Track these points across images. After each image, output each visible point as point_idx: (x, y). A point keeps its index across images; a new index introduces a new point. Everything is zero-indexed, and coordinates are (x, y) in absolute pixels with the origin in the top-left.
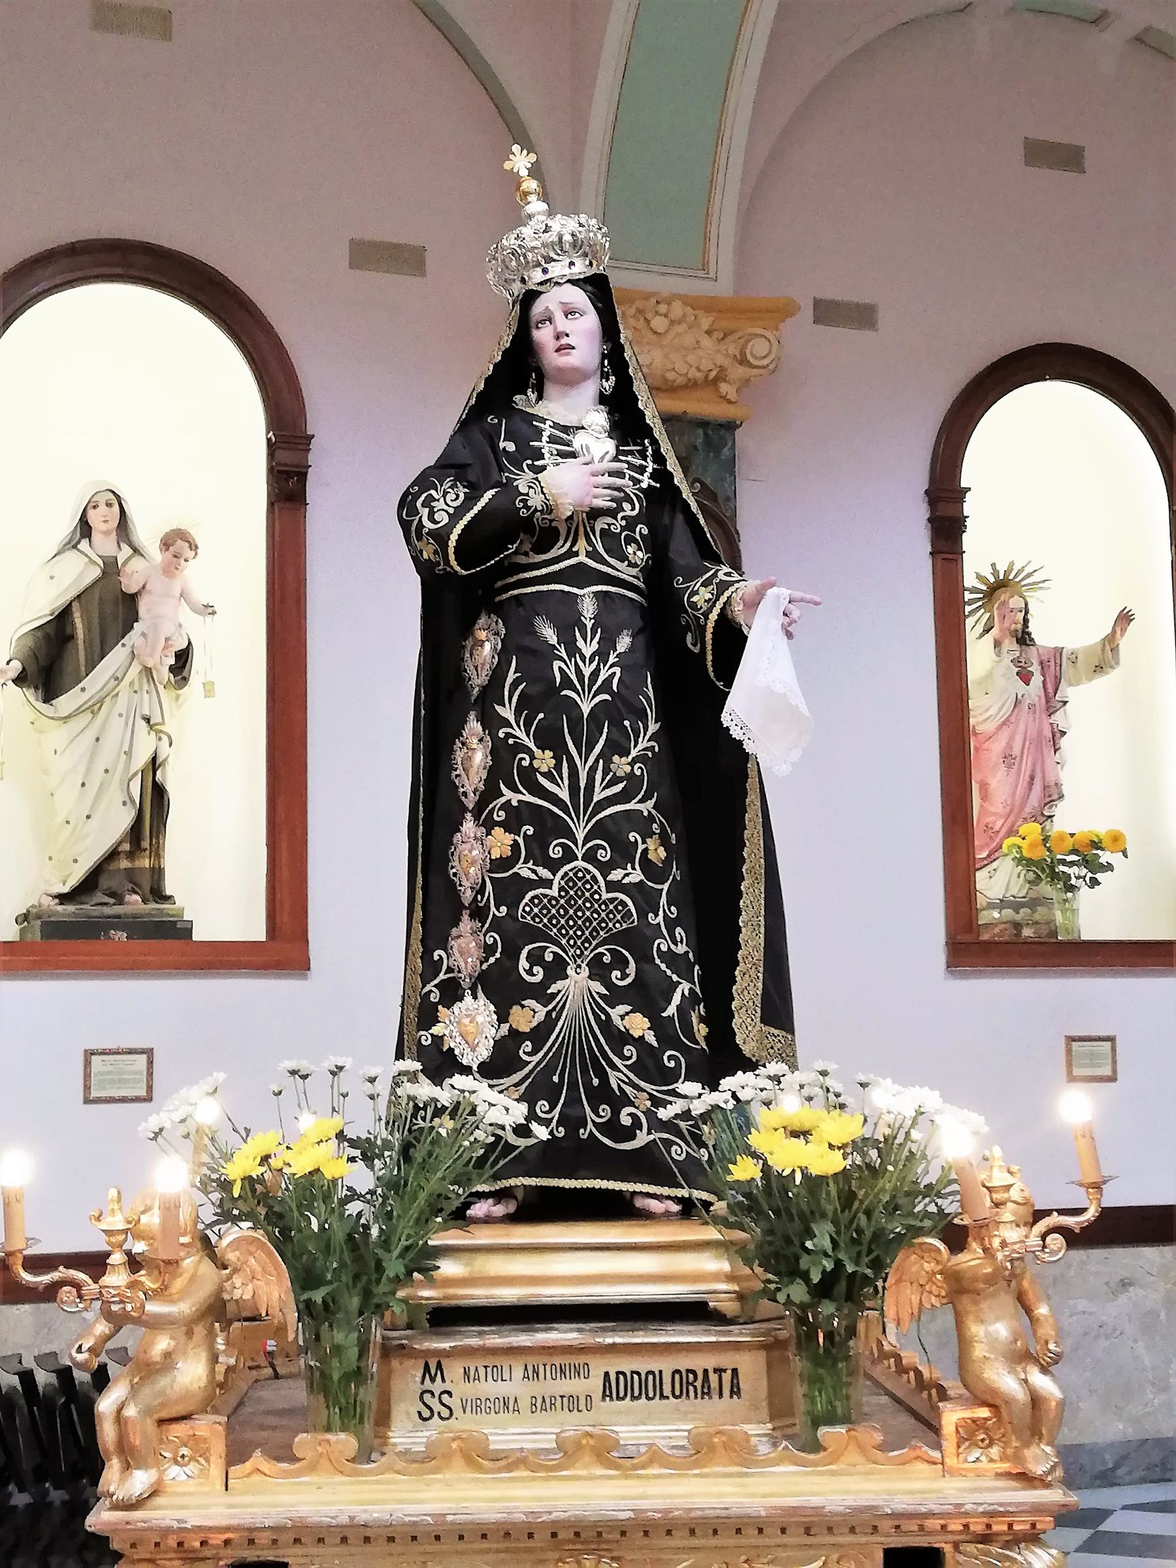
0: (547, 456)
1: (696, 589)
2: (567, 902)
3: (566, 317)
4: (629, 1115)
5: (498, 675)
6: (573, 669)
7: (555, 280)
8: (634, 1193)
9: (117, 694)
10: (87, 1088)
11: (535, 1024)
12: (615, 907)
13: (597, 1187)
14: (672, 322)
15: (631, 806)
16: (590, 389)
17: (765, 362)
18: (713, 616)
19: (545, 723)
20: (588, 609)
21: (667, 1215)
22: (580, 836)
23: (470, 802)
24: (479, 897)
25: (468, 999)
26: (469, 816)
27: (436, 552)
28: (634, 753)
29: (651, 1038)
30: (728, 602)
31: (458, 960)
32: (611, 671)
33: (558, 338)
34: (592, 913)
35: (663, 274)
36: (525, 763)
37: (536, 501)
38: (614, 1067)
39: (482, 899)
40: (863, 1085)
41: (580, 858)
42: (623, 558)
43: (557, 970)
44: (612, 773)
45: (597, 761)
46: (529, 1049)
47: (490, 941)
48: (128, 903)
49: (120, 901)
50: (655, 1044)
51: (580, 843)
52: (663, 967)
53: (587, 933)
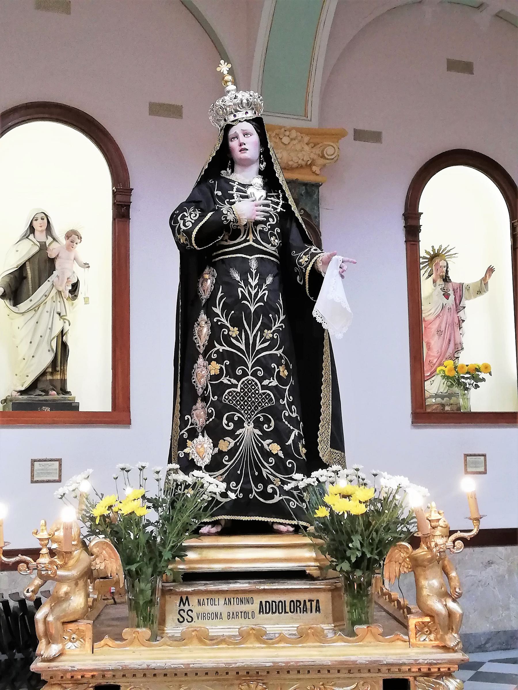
0: (235, 198)
7: (239, 120)
8: (273, 523)
9: (46, 302)
10: (32, 476)
11: (229, 448)
12: (266, 397)
14: (292, 139)
18: (309, 268)
19: (234, 315)
20: (254, 265)
21: (288, 532)
22: (250, 366)
23: (201, 350)
25: (200, 437)
26: (201, 356)
28: (274, 329)
29: (281, 454)
31: (195, 419)
32: (264, 293)
36: (226, 333)
40: (375, 475)
42: (269, 242)
43: (239, 424)
45: (257, 332)
47: (210, 411)
48: (51, 395)
49: (47, 393)
50: (283, 457)
51: (250, 368)
52: (286, 423)
53: (253, 408)
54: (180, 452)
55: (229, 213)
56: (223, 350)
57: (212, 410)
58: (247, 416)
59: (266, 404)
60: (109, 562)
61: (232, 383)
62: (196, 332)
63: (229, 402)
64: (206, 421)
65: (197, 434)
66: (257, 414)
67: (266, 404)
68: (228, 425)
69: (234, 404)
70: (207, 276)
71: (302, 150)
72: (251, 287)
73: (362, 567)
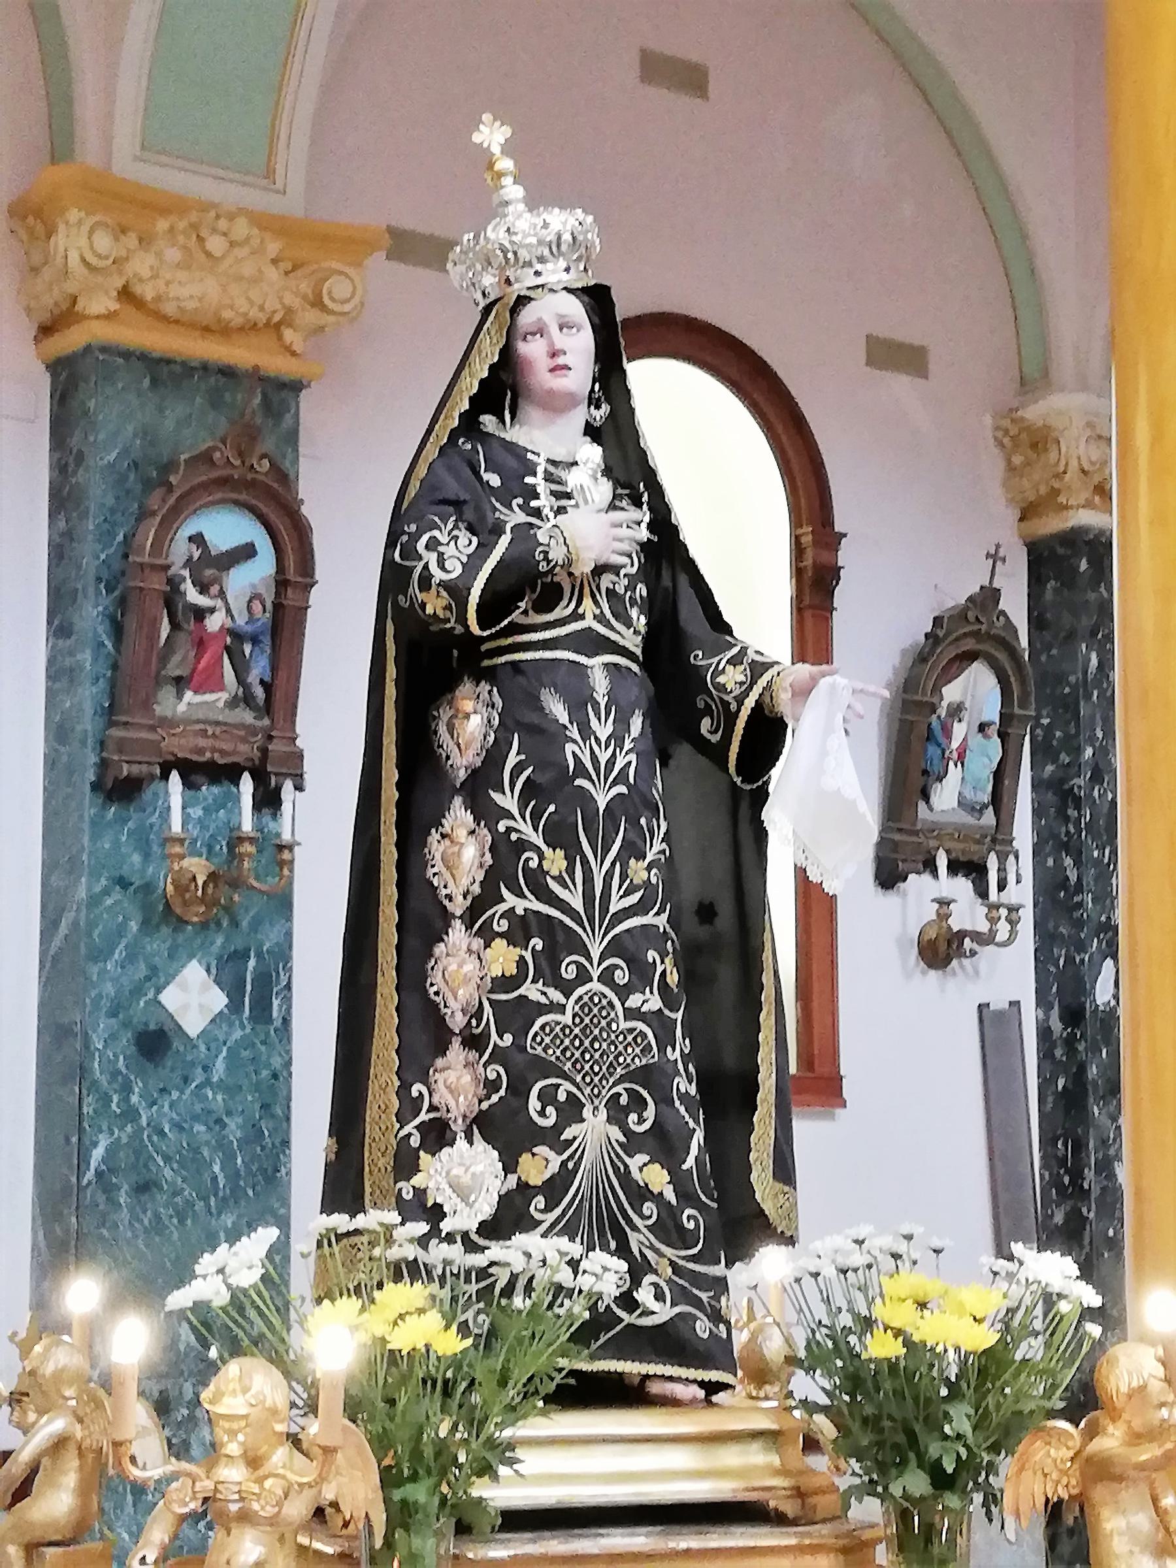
0: (542, 496)
1: (721, 667)
3: (561, 329)
4: (652, 1284)
5: (494, 757)
6: (587, 752)
7: (549, 286)
8: (646, 1377)
11: (547, 1175)
12: (635, 1039)
14: (232, 244)
15: (648, 919)
17: (347, 308)
18: (750, 702)
19: (556, 817)
20: (600, 684)
21: (693, 1402)
22: (595, 954)
23: (458, 906)
24: (474, 1022)
25: (461, 1143)
26: (458, 924)
28: (649, 857)
29: (670, 1195)
30: (769, 686)
31: (442, 1096)
32: (626, 759)
33: (554, 355)
34: (609, 1045)
36: (534, 864)
37: (557, 554)
38: (635, 1228)
39: (478, 1026)
41: (595, 978)
42: (628, 623)
43: (572, 1111)
45: (613, 864)
46: (542, 1206)
47: (492, 1076)
50: (674, 1201)
51: (595, 961)
52: (682, 1110)
53: (604, 1068)
54: (400, 1185)
56: (525, 910)
58: (592, 1090)
59: (637, 1060)
61: (552, 1002)
62: (438, 856)
63: (545, 1050)
64: (480, 1101)
65: (448, 1134)
66: (614, 1085)
67: (637, 1060)
68: (542, 1113)
69: (558, 1058)
70: (468, 705)
71: (257, 280)
73: (313, 1525)
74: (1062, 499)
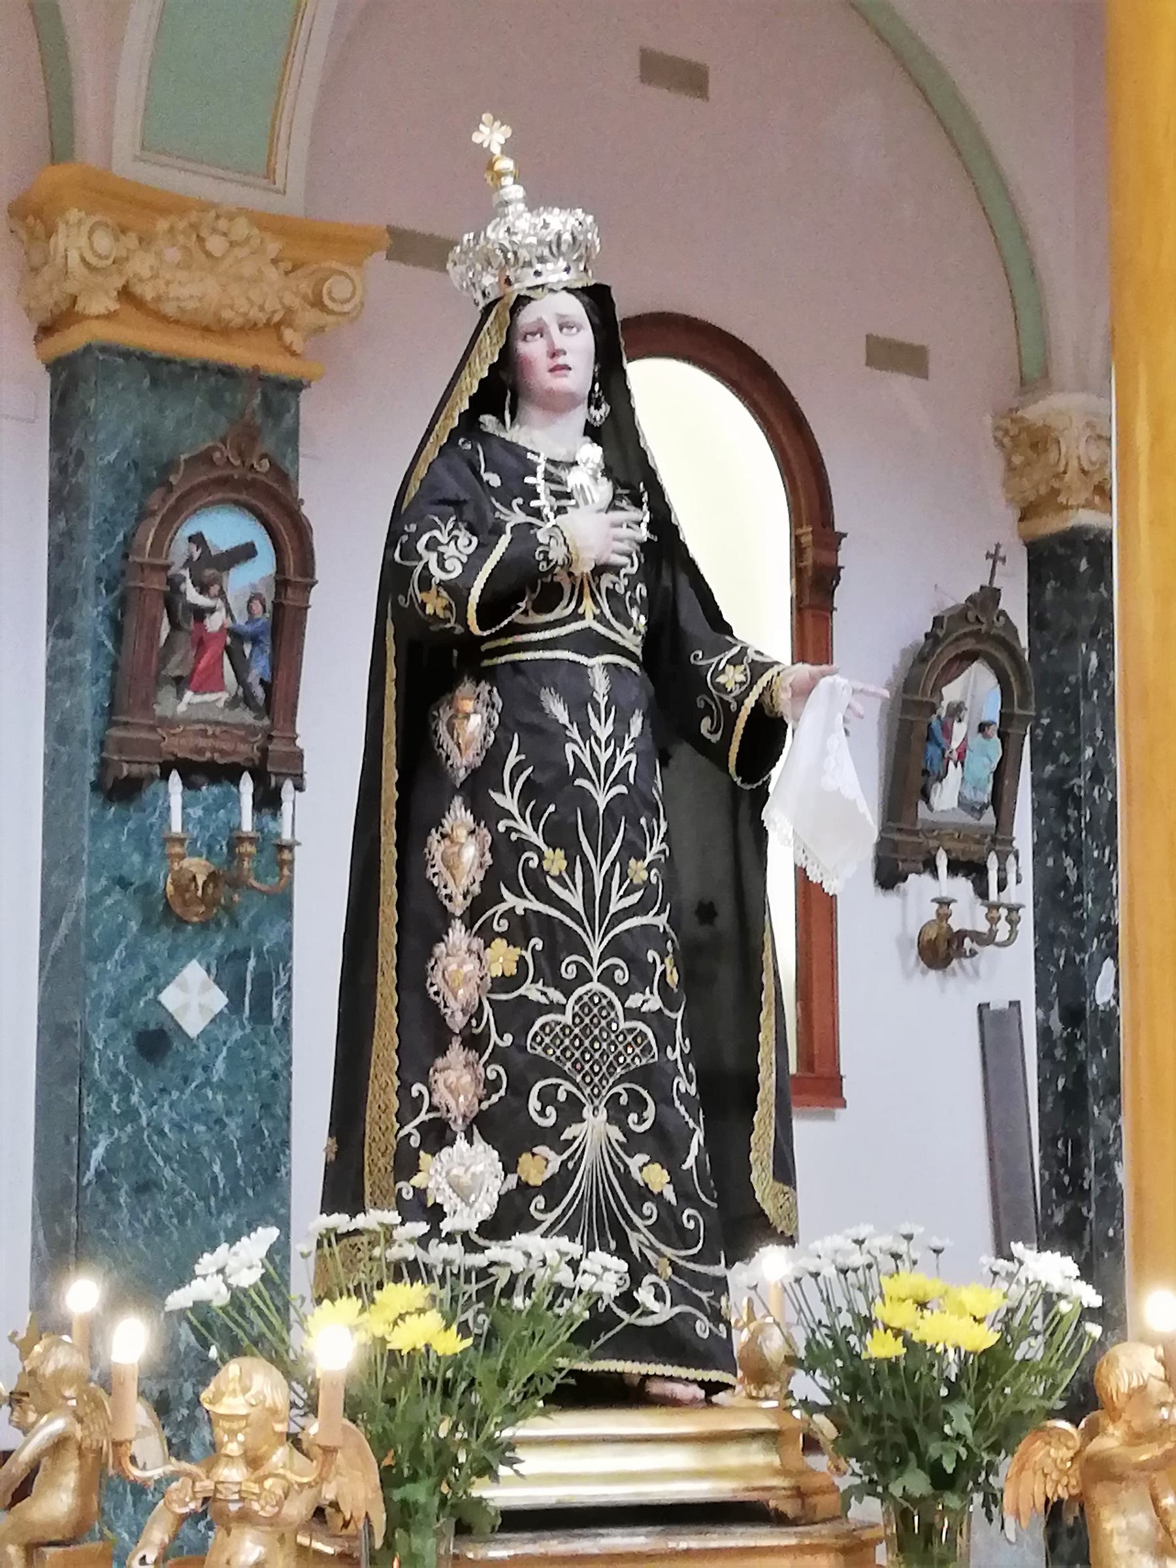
0: (542, 496)
1: (721, 667)
2: (583, 1031)
5: (494, 757)
8: (647, 1377)
11: (547, 1175)
12: (635, 1039)
13: (692, 1370)
14: (232, 244)
15: (648, 919)
16: (579, 416)
17: (347, 308)
18: (750, 702)
19: (556, 817)
20: (601, 684)
21: (692, 1403)
22: (595, 954)
23: (458, 906)
24: (474, 1022)
25: (461, 1143)
26: (458, 924)
27: (448, 608)
28: (649, 857)
29: (670, 1195)
31: (442, 1096)
35: (244, 184)
36: (534, 864)
37: (557, 554)
38: (635, 1228)
39: (478, 1026)
40: (937, 1251)
41: (595, 978)
42: (628, 623)
43: (572, 1111)
44: (628, 881)
45: (613, 864)
46: (542, 1206)
47: (492, 1076)
50: (674, 1201)
51: (595, 961)
52: (682, 1110)
54: (400, 1184)
55: (553, 542)
56: (525, 910)
57: (498, 1073)
60: (346, 1480)
61: (552, 1002)
62: (438, 856)
63: (545, 1050)
64: (480, 1101)
65: (448, 1134)
66: (610, 1088)
67: (637, 1060)
68: (542, 1113)
69: (558, 1058)
70: (468, 705)
72: (597, 740)
74: (1062, 499)
